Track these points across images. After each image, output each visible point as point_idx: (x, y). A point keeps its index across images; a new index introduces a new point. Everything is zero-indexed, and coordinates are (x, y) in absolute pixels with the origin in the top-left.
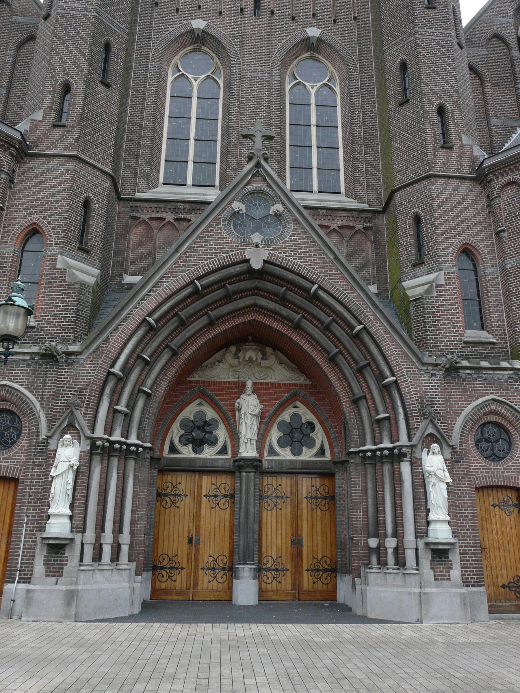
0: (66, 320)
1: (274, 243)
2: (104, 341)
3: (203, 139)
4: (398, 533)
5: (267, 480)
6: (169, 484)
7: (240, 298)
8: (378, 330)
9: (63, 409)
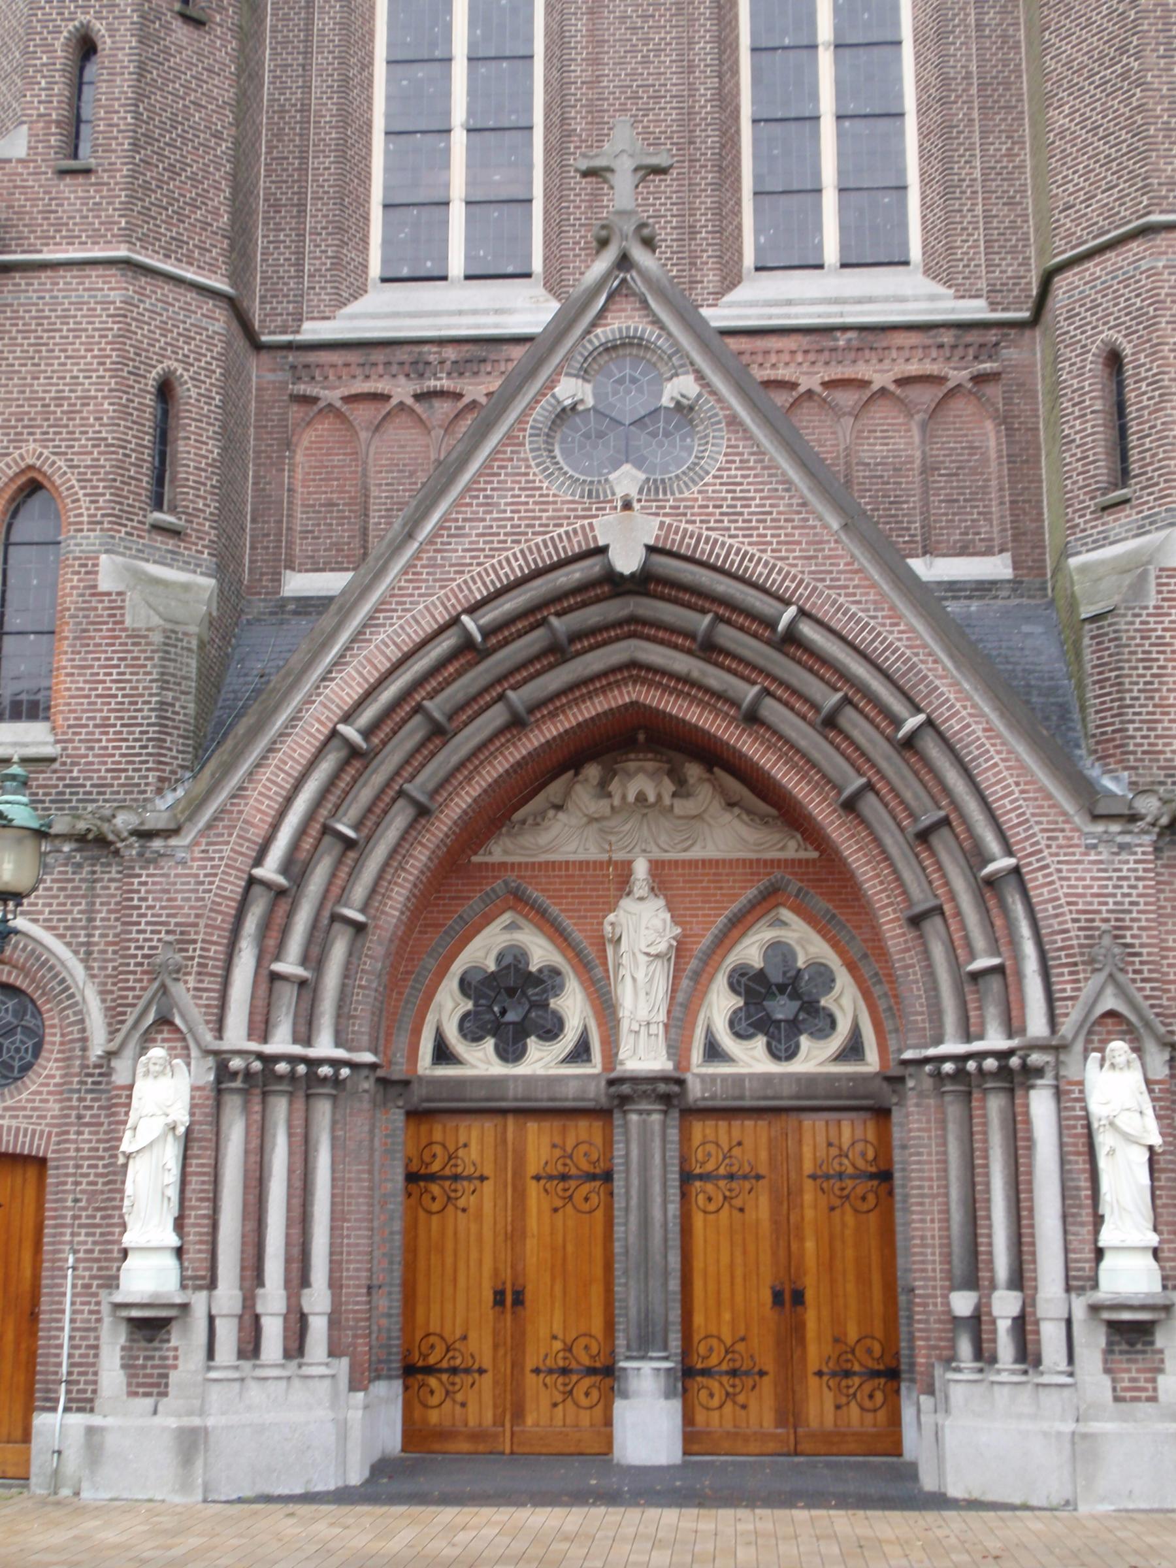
0: (133, 733)
1: (673, 493)
2: (234, 796)
3: (491, 124)
4: (1020, 1279)
5: (700, 1130)
6: (437, 1149)
7: (592, 648)
8: (968, 726)
9: (141, 981)
